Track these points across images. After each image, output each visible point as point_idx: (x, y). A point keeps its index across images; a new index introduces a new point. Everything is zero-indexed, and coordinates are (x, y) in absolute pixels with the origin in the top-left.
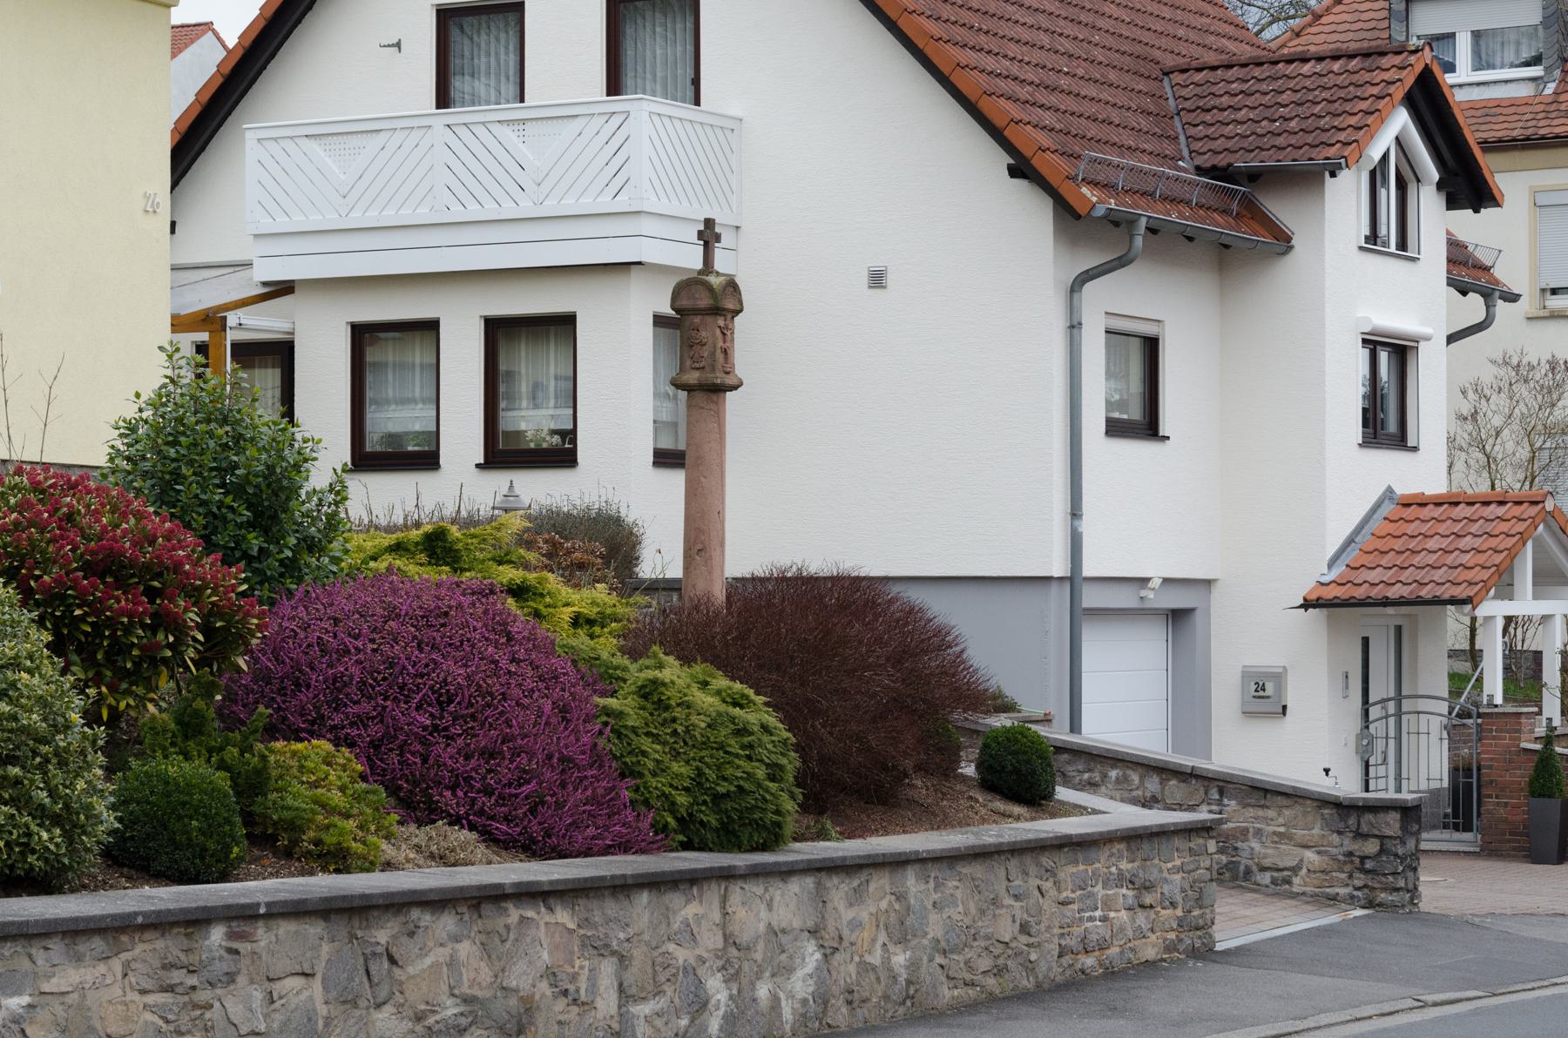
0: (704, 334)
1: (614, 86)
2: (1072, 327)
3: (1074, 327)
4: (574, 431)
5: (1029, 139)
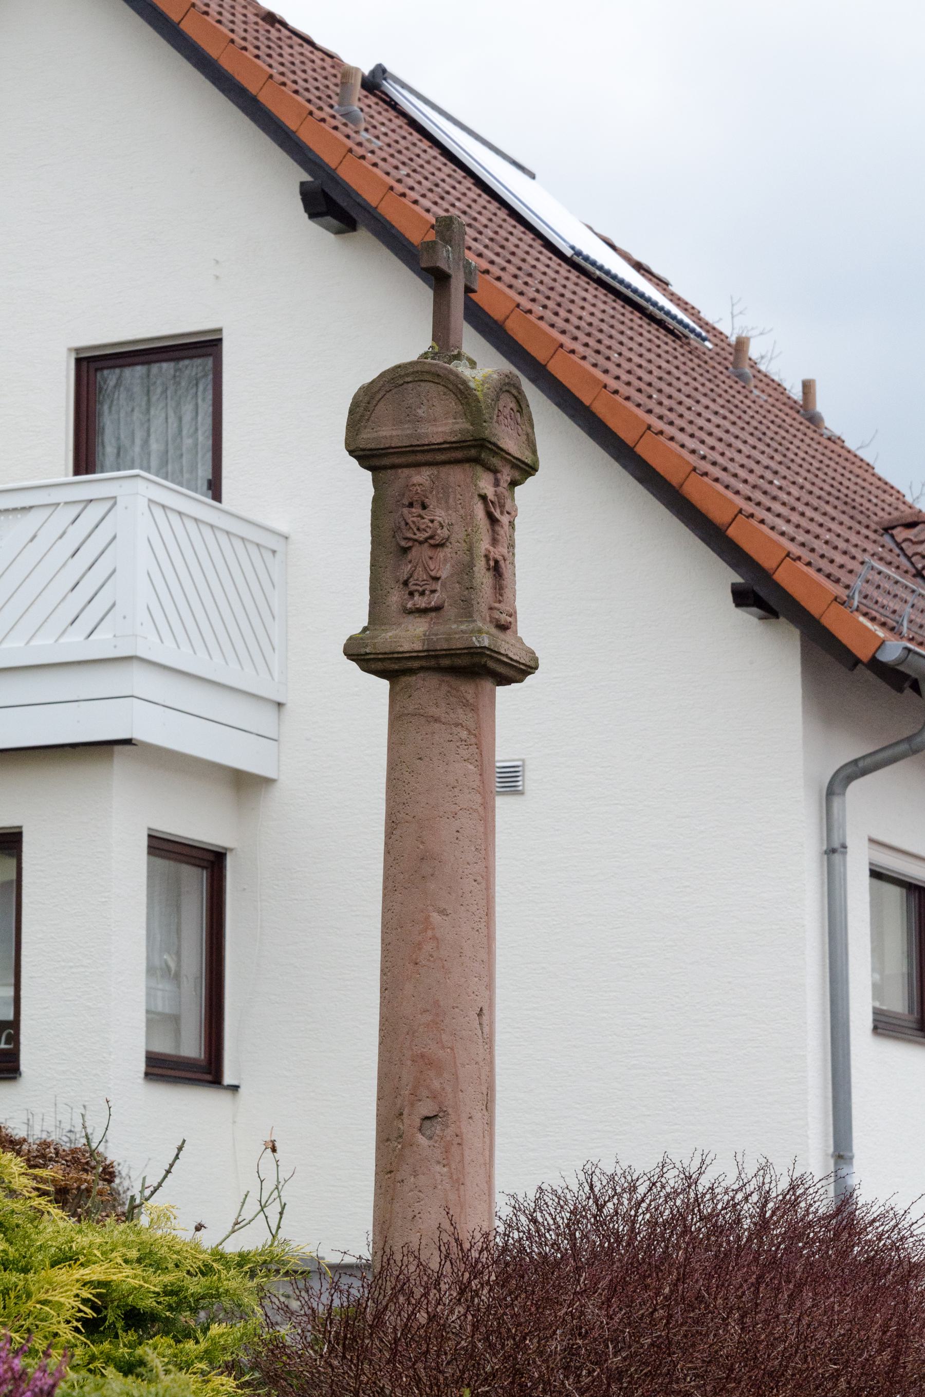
0: (440, 514)
1: (85, 460)
2: (831, 851)
3: (833, 851)
4: (15, 1024)
5: (763, 541)
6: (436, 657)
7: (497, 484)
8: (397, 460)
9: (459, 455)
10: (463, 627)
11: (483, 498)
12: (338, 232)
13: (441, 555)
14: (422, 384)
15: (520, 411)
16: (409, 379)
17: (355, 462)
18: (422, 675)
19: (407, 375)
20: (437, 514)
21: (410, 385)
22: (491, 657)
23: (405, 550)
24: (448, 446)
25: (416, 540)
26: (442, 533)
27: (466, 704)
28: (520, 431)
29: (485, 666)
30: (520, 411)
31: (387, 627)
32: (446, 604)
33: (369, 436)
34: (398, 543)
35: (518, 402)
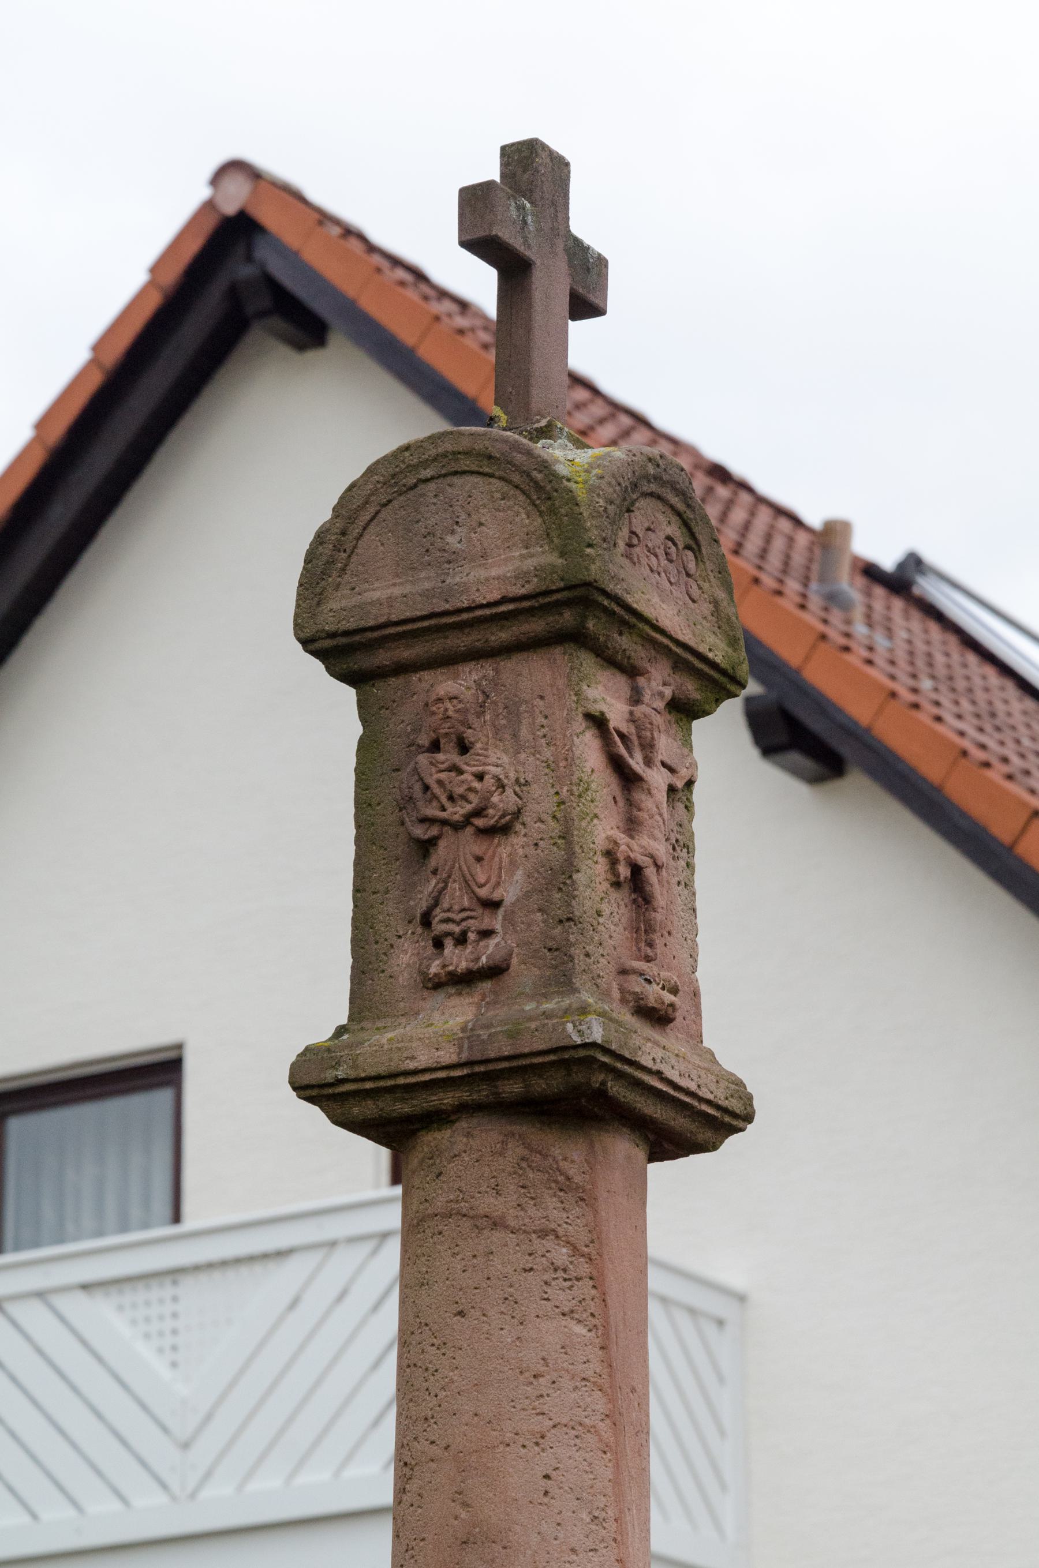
0: (496, 759)
6: (489, 1077)
7: (636, 698)
8: (406, 653)
9: (536, 626)
10: (549, 1006)
11: (598, 722)
12: (814, 780)
13: (504, 852)
14: (456, 480)
15: (694, 546)
16: (427, 473)
17: (317, 666)
18: (463, 1124)
19: (425, 464)
20: (493, 759)
21: (432, 486)
22: (620, 1075)
23: (426, 847)
24: (511, 607)
25: (444, 822)
26: (503, 802)
27: (565, 1186)
28: (695, 592)
29: (601, 1094)
30: (694, 546)
31: (388, 1022)
32: (514, 961)
33: (344, 603)
34: (411, 833)
35: (686, 524)
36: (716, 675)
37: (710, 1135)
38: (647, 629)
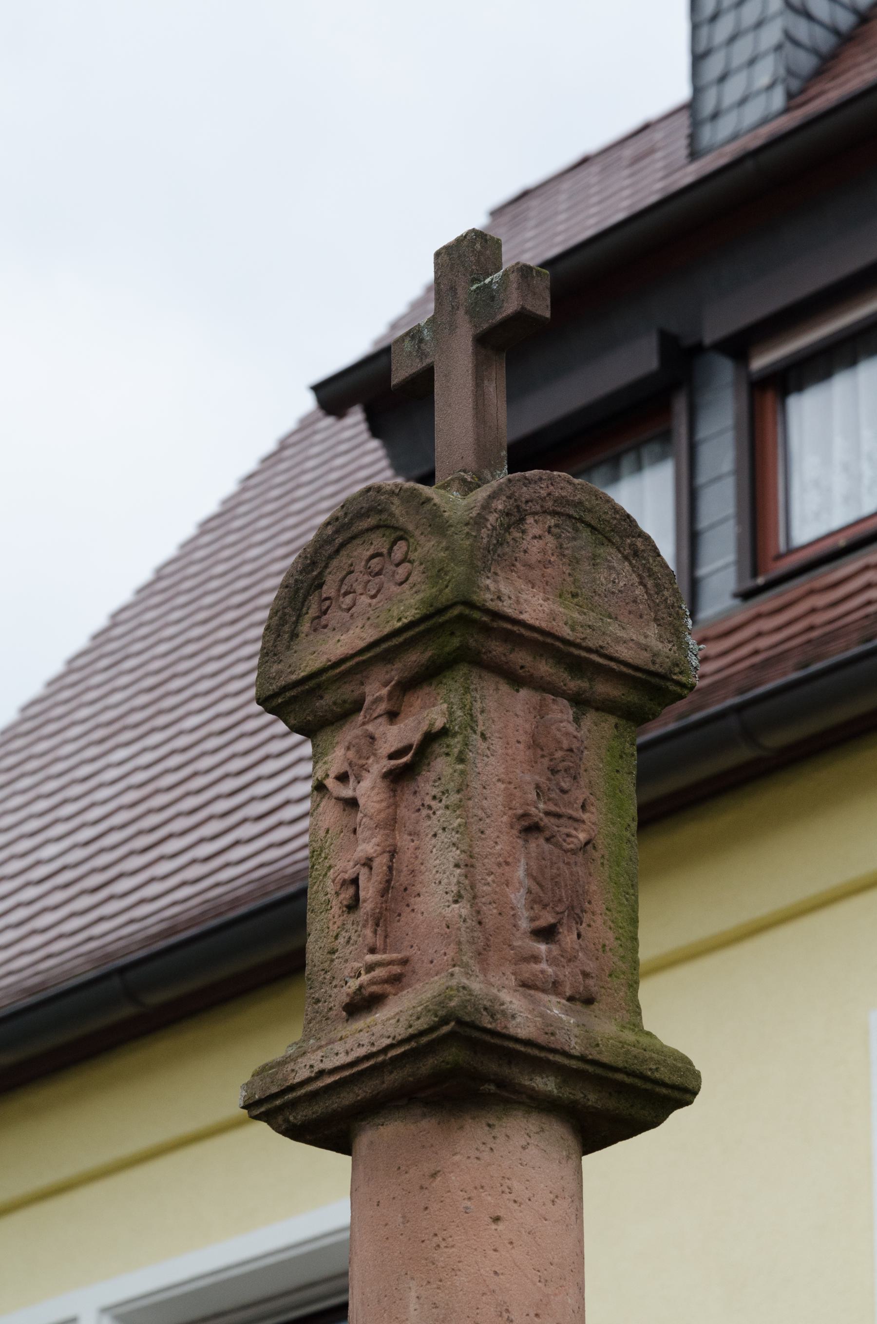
36: (422, 628)
37: (431, 1061)
38: (331, 673)
